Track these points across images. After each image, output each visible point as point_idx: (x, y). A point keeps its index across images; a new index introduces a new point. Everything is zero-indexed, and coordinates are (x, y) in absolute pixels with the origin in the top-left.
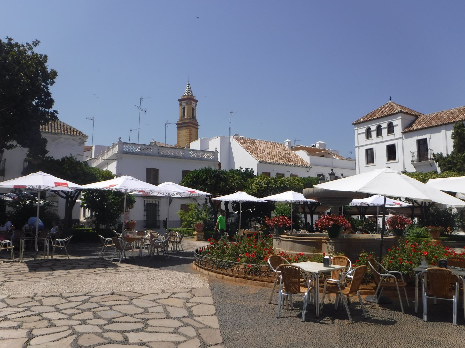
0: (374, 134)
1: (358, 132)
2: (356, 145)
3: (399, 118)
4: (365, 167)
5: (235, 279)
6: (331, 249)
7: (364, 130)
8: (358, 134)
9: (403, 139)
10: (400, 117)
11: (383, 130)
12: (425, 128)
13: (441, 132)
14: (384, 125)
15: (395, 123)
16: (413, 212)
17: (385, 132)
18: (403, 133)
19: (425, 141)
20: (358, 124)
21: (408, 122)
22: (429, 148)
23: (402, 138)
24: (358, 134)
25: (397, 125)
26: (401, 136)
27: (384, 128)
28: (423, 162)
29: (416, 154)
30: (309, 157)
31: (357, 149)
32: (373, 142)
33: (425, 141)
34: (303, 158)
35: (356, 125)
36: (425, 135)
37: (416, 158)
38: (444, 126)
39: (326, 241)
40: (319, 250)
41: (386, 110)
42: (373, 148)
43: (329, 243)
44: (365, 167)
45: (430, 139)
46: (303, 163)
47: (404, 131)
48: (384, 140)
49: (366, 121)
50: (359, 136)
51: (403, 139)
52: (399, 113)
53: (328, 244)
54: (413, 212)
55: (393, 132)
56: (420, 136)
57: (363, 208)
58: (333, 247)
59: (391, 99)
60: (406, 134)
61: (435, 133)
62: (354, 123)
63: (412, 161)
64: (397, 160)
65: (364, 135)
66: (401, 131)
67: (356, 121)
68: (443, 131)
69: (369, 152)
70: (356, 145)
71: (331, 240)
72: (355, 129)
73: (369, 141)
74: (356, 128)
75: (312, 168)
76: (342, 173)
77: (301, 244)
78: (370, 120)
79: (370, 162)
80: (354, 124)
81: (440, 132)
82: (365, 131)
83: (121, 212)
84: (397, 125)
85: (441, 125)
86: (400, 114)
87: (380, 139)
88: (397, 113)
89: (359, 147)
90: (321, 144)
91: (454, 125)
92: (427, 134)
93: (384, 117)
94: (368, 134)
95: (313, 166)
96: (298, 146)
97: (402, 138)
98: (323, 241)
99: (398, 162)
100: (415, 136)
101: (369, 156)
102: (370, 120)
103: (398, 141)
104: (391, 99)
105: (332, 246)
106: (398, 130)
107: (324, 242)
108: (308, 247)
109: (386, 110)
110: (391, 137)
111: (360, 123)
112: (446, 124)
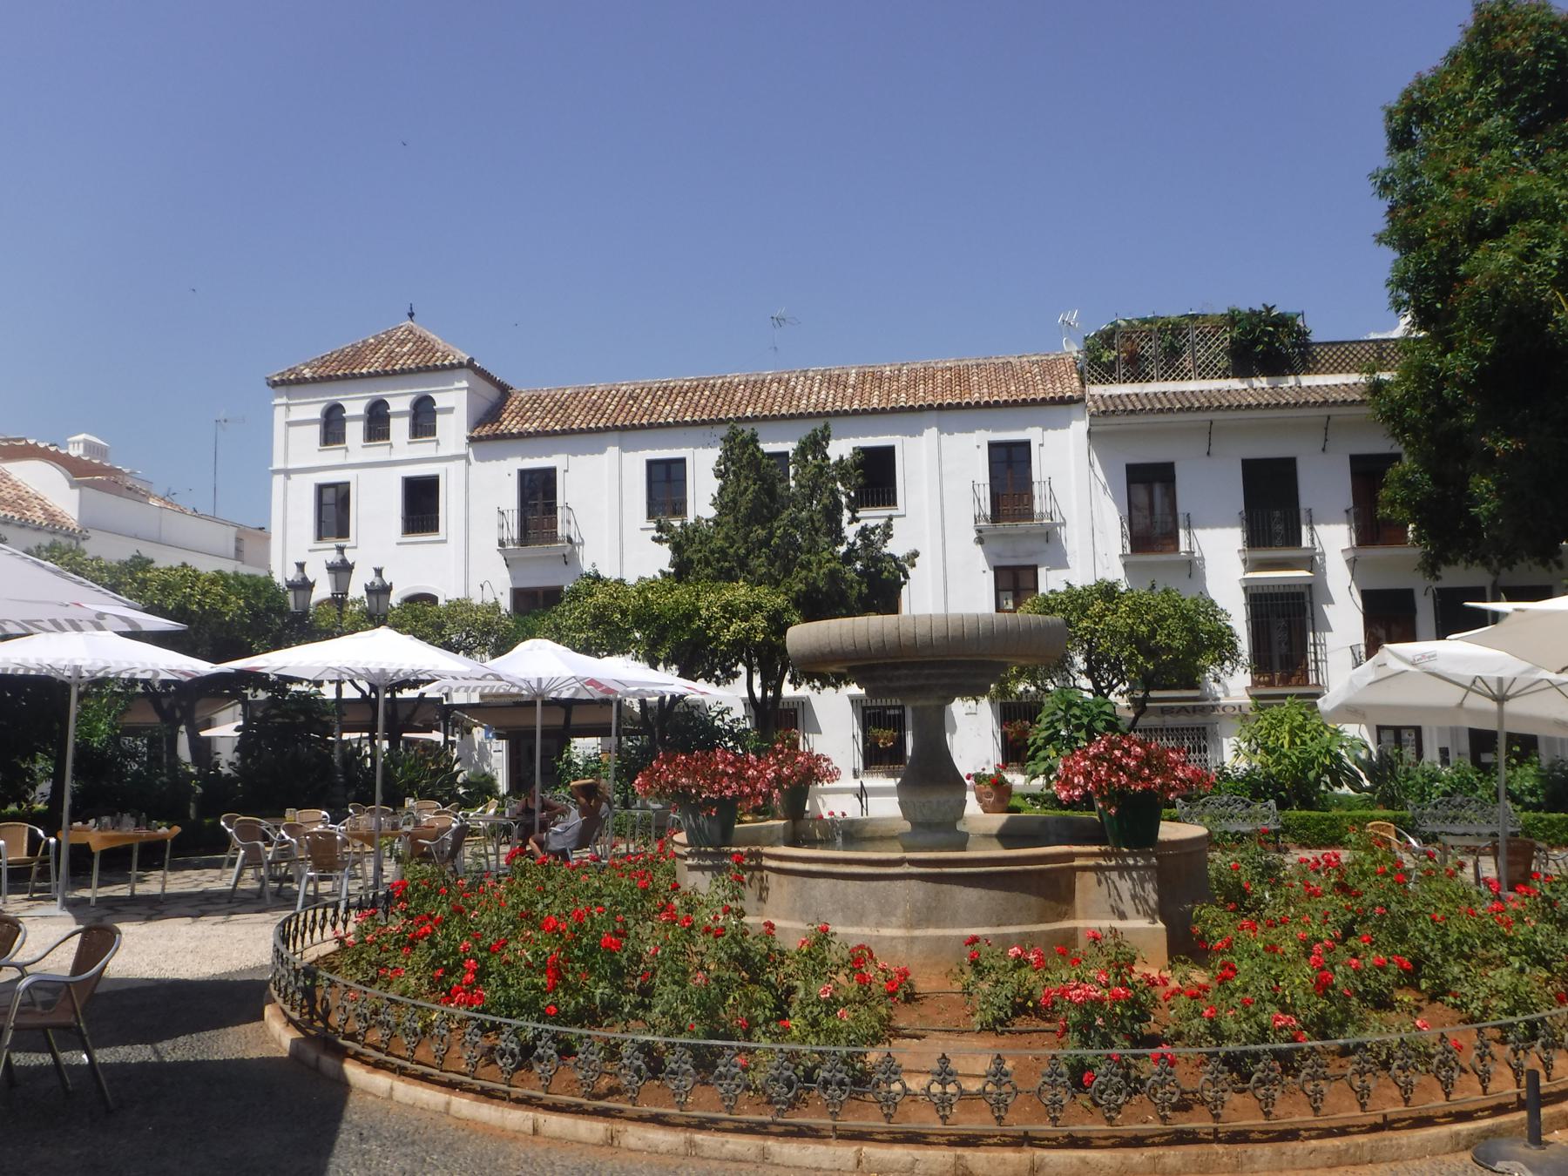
0: (355, 431)
1: (287, 415)
2: (278, 464)
3: (457, 385)
4: (398, 544)
5: (958, 1157)
6: (1134, 897)
7: (315, 411)
8: (290, 424)
9: (468, 462)
10: (465, 384)
11: (348, 425)
12: (554, 433)
13: (606, 455)
14: (400, 403)
15: (441, 400)
16: (567, 720)
17: (400, 427)
18: (472, 440)
19: (548, 476)
20: (290, 383)
21: (484, 405)
22: (560, 503)
23: (466, 457)
24: (290, 424)
25: (450, 410)
26: (463, 451)
27: (400, 414)
28: (534, 550)
29: (513, 519)
30: (76, 492)
31: (278, 480)
32: (351, 460)
33: (548, 476)
34: (42, 493)
35: (283, 389)
36: (548, 455)
37: (514, 533)
38: (616, 435)
39: (1104, 863)
40: (1064, 908)
41: (405, 350)
42: (348, 483)
43: (1123, 870)
44: (398, 544)
45: (566, 471)
46: (51, 516)
47: (475, 434)
48: (394, 457)
49: (329, 379)
50: (292, 429)
51: (468, 462)
52: (461, 365)
53: (1114, 875)
54: (567, 720)
55: (343, 441)
56: (531, 457)
57: (898, 707)
58: (1149, 887)
59: (411, 315)
60: (480, 445)
61: (489, 460)
62: (276, 379)
63: (501, 543)
64: (441, 535)
65: (315, 431)
66: (464, 432)
67: (283, 374)
68: (613, 451)
69: (329, 495)
70: (278, 464)
71: (1134, 856)
72: (278, 401)
73: (334, 456)
74: (284, 400)
75: (88, 538)
76: (378, 566)
77: (984, 887)
78: (345, 377)
79: (330, 535)
80: (275, 384)
81: (602, 451)
82: (318, 416)
83: (695, 719)
84: (450, 410)
85: (607, 429)
86: (465, 372)
87: (378, 452)
88: (452, 367)
89: (287, 473)
90: (89, 447)
91: (724, 431)
92: (556, 452)
93: (403, 372)
94: (332, 428)
95: (91, 533)
96: (14, 440)
97: (466, 457)
98: (1078, 862)
99: (445, 542)
100: (514, 455)
101: (331, 511)
102: (345, 377)
103: (451, 465)
104: (411, 315)
105: (1142, 881)
106: (453, 427)
107: (1085, 869)
108: (1020, 898)
109: (405, 350)
110: (424, 448)
111: (301, 381)
112: (624, 428)
